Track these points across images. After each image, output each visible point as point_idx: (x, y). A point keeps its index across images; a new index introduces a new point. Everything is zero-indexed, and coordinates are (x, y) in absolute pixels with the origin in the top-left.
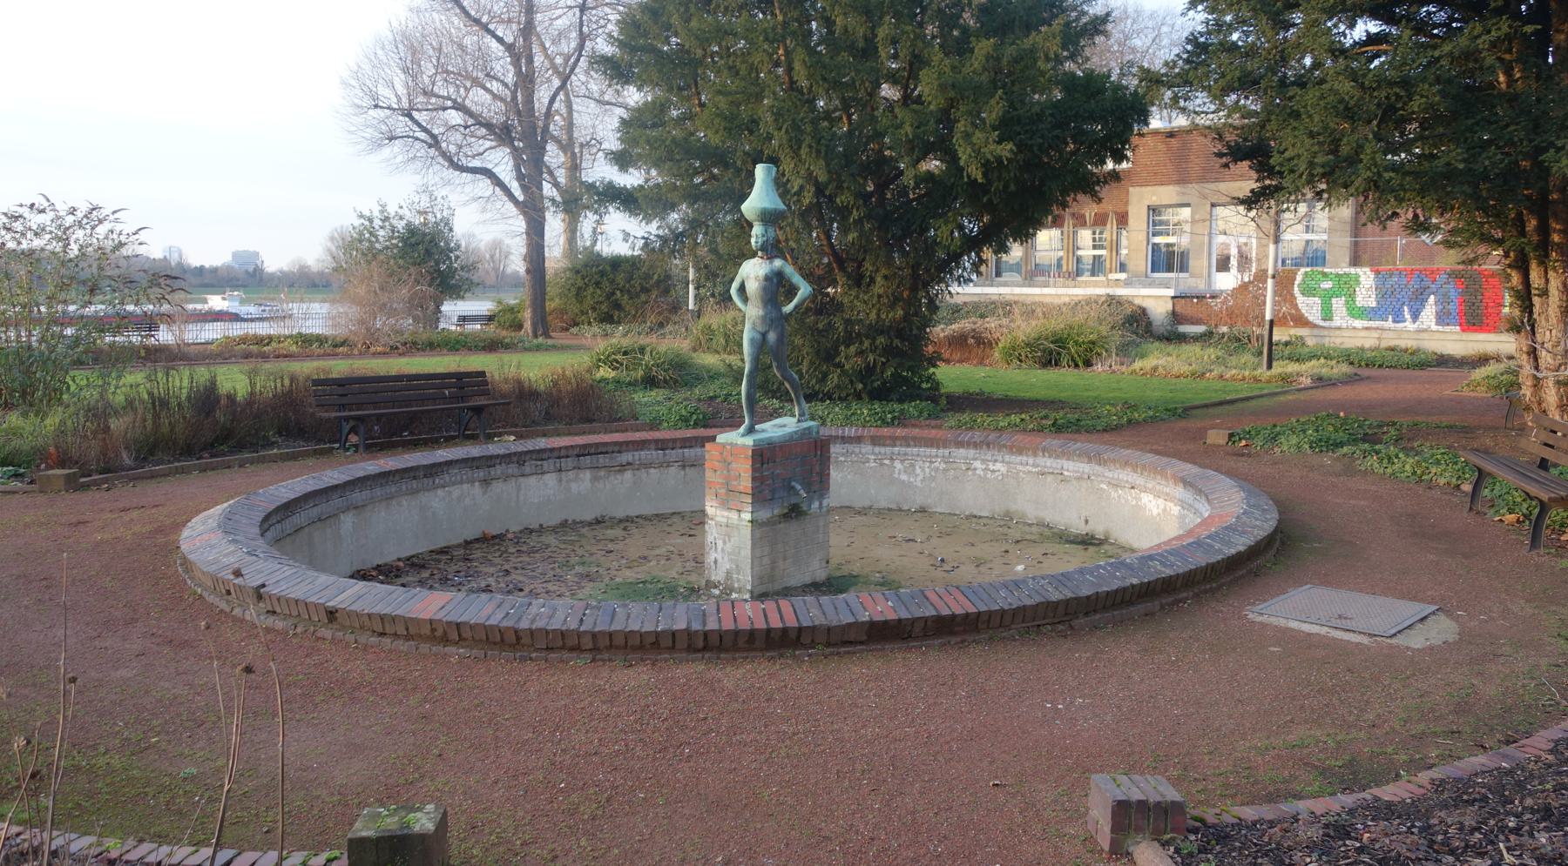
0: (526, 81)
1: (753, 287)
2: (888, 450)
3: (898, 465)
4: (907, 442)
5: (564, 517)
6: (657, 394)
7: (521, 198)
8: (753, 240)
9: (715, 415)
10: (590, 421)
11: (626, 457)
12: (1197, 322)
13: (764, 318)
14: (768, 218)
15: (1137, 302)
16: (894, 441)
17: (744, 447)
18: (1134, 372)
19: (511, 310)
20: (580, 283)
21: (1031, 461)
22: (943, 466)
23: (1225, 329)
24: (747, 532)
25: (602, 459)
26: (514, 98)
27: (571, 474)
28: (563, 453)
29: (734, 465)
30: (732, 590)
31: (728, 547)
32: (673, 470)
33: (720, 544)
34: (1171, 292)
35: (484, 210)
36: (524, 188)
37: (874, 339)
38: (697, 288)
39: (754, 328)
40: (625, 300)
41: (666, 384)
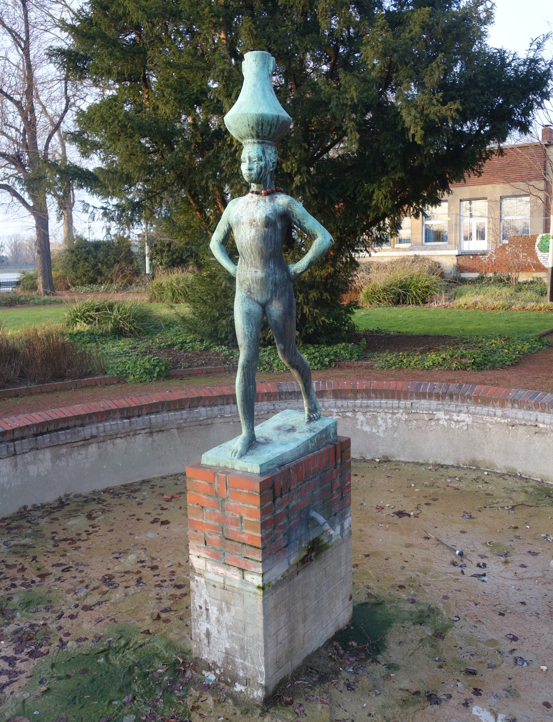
0: (30, 125)
1: (246, 237)
2: (350, 402)
3: (360, 417)
4: (368, 393)
5: (22, 504)
6: (124, 344)
7: (31, 204)
8: (244, 168)
9: (175, 364)
10: (62, 377)
11: (90, 430)
12: (473, 271)
13: (264, 282)
14: (264, 130)
15: (435, 259)
16: (355, 393)
17: (246, 475)
18: (460, 307)
19: (31, 277)
20: (74, 259)
21: (499, 412)
22: (405, 417)
23: (491, 275)
24: (256, 601)
25: (63, 436)
26: (24, 140)
27: (28, 457)
28: (17, 434)
29: (232, 503)
30: (235, 679)
31: (227, 618)
32: (140, 438)
33: (214, 611)
34: (456, 252)
35: (7, 212)
36: (32, 197)
37: (307, 294)
38: (151, 260)
39: (249, 297)
40: (104, 269)
41: (131, 334)
